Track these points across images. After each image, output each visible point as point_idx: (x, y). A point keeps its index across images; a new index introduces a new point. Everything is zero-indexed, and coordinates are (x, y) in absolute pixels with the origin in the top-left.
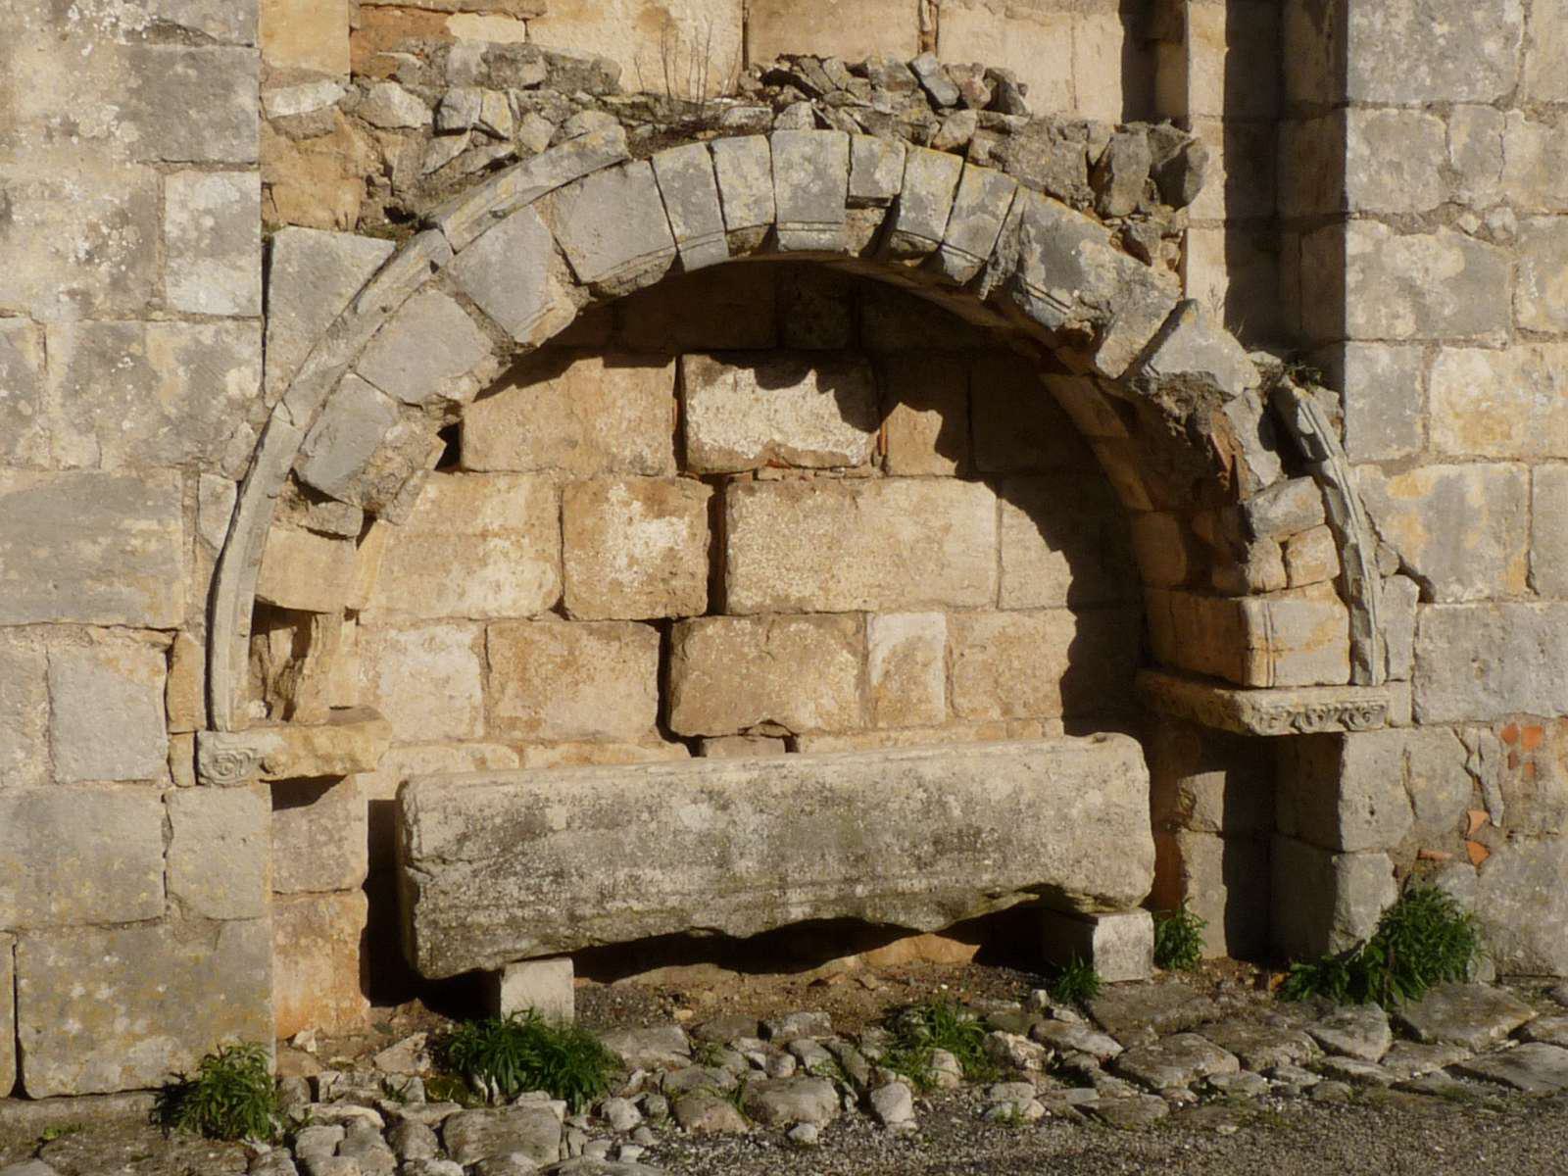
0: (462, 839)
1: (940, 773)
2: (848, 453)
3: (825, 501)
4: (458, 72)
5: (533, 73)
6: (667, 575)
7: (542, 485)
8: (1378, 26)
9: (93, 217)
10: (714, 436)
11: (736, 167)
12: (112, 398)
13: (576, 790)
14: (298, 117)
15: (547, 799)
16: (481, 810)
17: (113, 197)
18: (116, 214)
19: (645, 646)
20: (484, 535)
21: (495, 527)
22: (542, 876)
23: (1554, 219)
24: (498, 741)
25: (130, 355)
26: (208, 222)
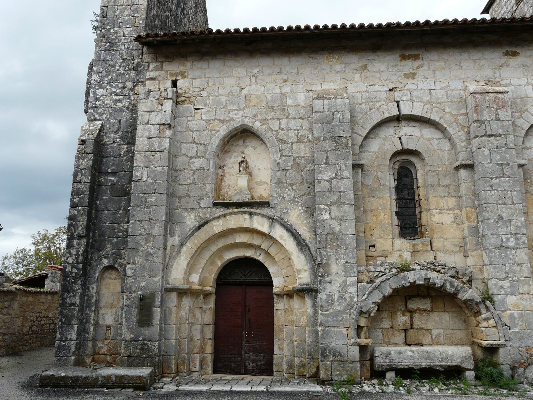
0: (381, 354)
5: (386, 264)
11: (410, 274)
17: (342, 280)
20: (382, 318)
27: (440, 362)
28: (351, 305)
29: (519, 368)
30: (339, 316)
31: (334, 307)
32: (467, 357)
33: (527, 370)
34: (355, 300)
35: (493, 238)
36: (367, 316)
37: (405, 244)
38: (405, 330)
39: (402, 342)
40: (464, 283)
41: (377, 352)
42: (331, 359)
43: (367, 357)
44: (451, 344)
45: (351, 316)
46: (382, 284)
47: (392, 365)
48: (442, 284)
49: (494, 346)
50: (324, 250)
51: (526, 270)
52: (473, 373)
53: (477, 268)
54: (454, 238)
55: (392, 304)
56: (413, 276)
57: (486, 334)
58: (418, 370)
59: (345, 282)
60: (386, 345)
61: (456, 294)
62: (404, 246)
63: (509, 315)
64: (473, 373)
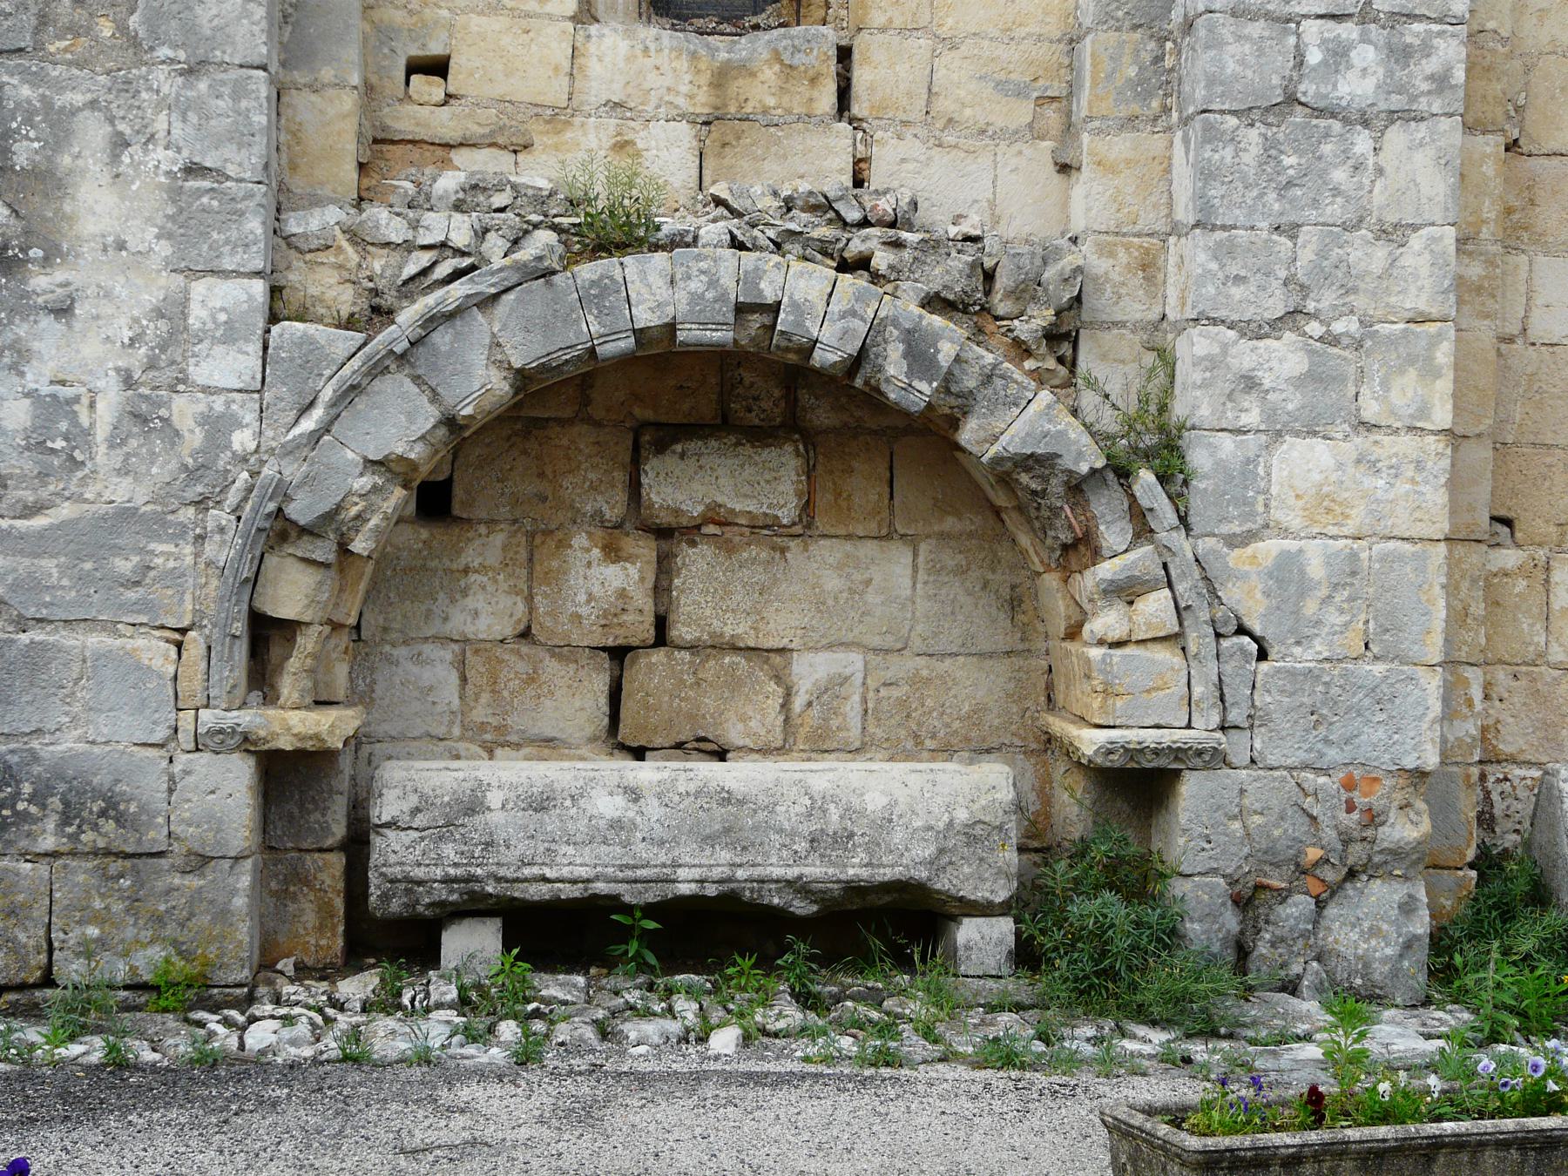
0: (416, 811)
1: (826, 784)
2: (780, 514)
3: (758, 554)
4: (441, 198)
5: (499, 200)
6: (619, 611)
7: (516, 532)
8: (1228, 160)
9: (136, 313)
10: (662, 496)
11: (643, 274)
12: (144, 450)
13: (515, 780)
14: (305, 235)
15: (489, 784)
16: (433, 790)
17: (151, 298)
18: (152, 310)
19: (598, 669)
20: (466, 571)
21: (476, 564)
22: (476, 845)
23: (1402, 326)
24: (472, 741)
25: (158, 417)
26: (223, 317)
27: (797, 858)
28: (210, 477)
29: (1283, 896)
30: (117, 550)
31: (83, 482)
32: (978, 830)
33: (1331, 911)
34: (243, 440)
35: (1239, 38)
36: (324, 550)
37: (663, 60)
38: (619, 654)
39: (589, 730)
40: (1022, 350)
41: (390, 795)
42: (48, 842)
43: (326, 830)
44: (910, 744)
45: (210, 549)
46: (442, 338)
47: (476, 879)
48: (853, 348)
49: (1149, 763)
50: (24, 72)
51: (1425, 271)
52: (1004, 928)
53: (1127, 247)
54: (1008, 35)
55: (541, 475)
56: (659, 283)
57: (1105, 683)
58: (650, 910)
59: (173, 312)
60: (475, 749)
61: (954, 423)
62: (653, 80)
63: (1269, 563)
64: (1004, 928)
